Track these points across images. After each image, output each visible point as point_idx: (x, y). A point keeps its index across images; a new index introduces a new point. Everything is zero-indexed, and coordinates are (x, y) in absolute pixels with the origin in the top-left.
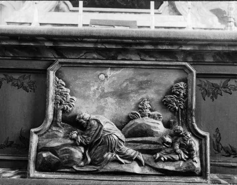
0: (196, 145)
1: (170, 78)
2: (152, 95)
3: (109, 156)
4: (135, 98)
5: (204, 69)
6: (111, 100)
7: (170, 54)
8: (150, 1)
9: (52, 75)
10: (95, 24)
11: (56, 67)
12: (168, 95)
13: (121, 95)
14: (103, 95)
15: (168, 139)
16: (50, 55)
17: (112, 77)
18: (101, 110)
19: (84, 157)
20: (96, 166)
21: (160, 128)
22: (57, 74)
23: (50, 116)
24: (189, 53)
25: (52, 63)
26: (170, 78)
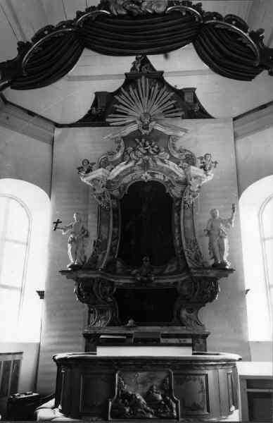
0: (174, 406)
1: (163, 375)
2: (156, 383)
3: (139, 410)
4: (149, 385)
5: (176, 372)
6: (140, 386)
7: (164, 366)
8: (192, 39)
9: (117, 375)
10: (49, 184)
11: (119, 372)
12: (25, 398)
13: (144, 383)
14: (137, 383)
15: (163, 402)
16: (116, 367)
17: (141, 375)
18: (136, 390)
19: (130, 412)
20: (134, 416)
21: (160, 398)
22: (119, 375)
23: (116, 394)
24: (169, 366)
25: (116, 370)
26: (163, 375)
